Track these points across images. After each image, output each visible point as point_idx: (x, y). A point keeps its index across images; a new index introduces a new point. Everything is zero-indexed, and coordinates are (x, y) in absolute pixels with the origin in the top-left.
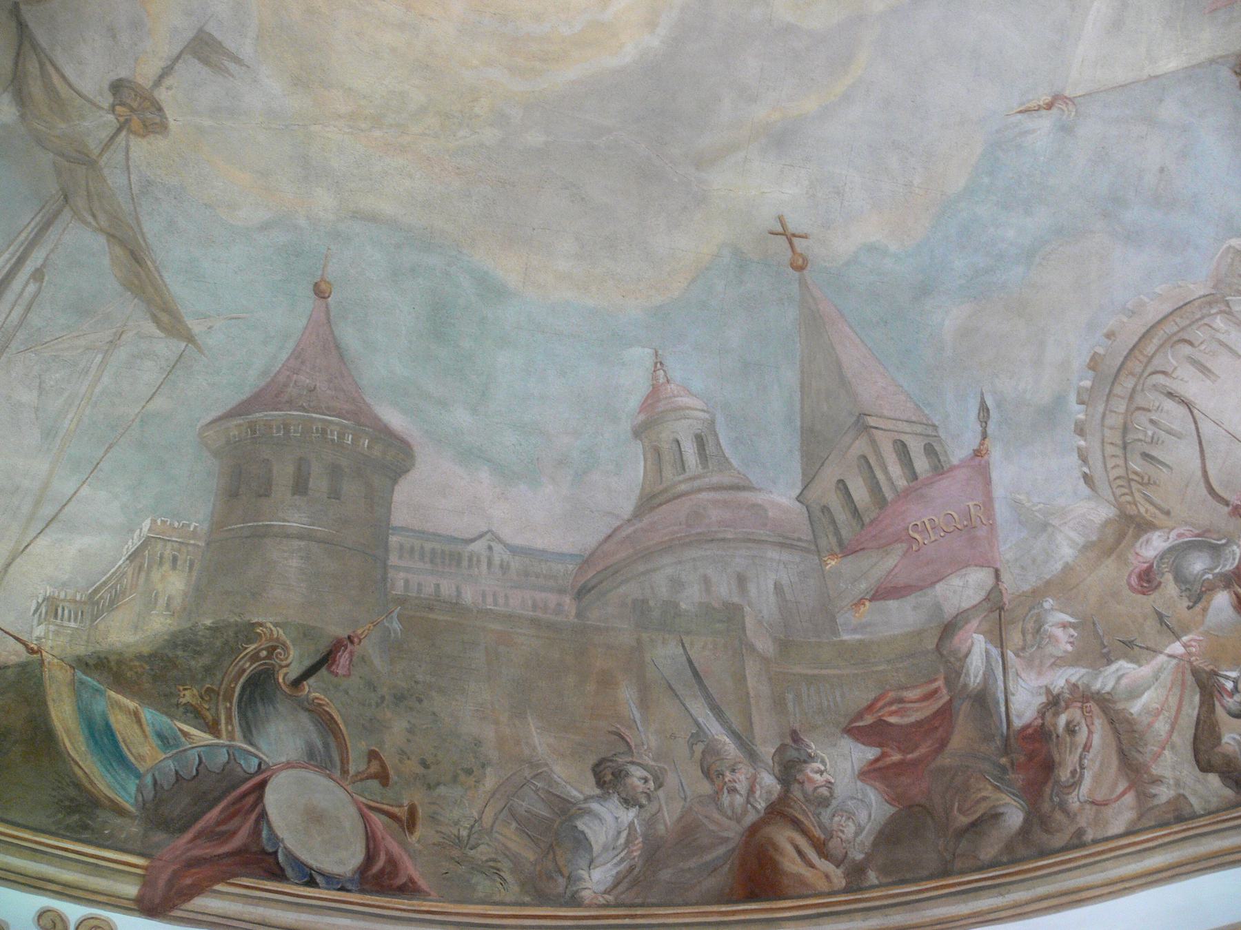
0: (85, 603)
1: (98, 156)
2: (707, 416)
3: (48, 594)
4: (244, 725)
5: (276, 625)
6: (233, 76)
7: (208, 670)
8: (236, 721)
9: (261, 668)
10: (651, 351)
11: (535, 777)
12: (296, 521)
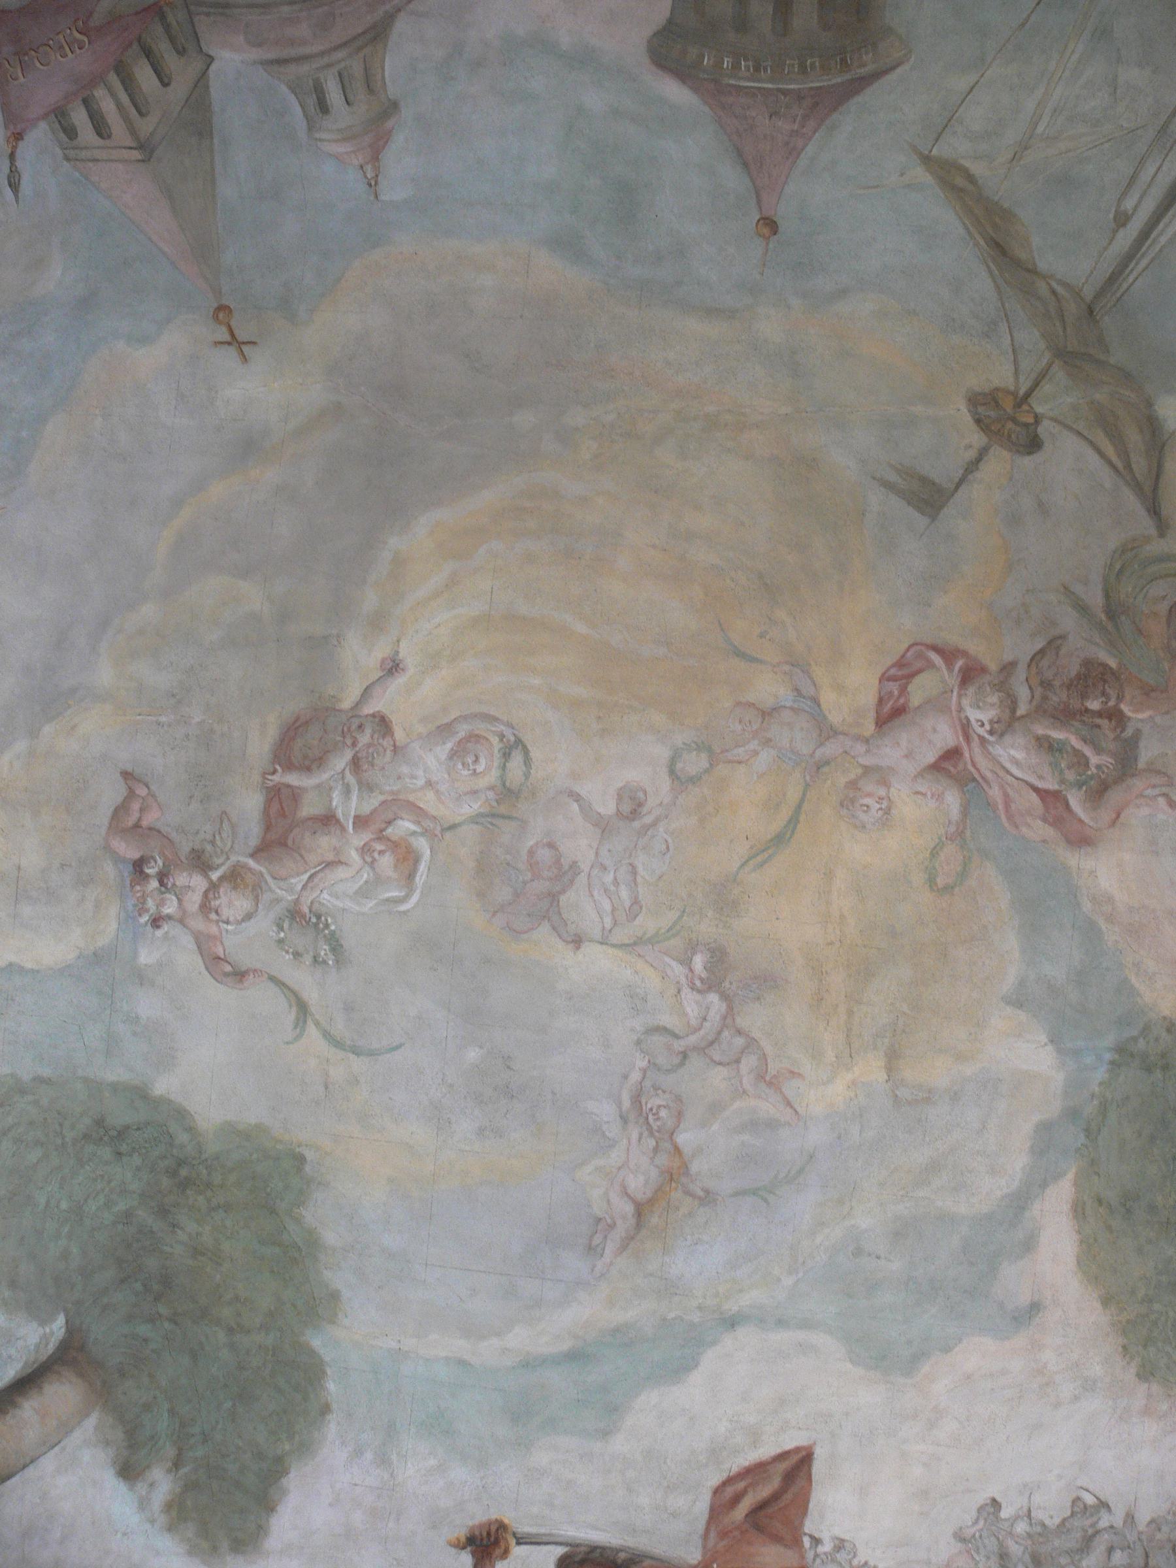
1: (1053, 363)
2: (317, 136)
10: (382, 197)
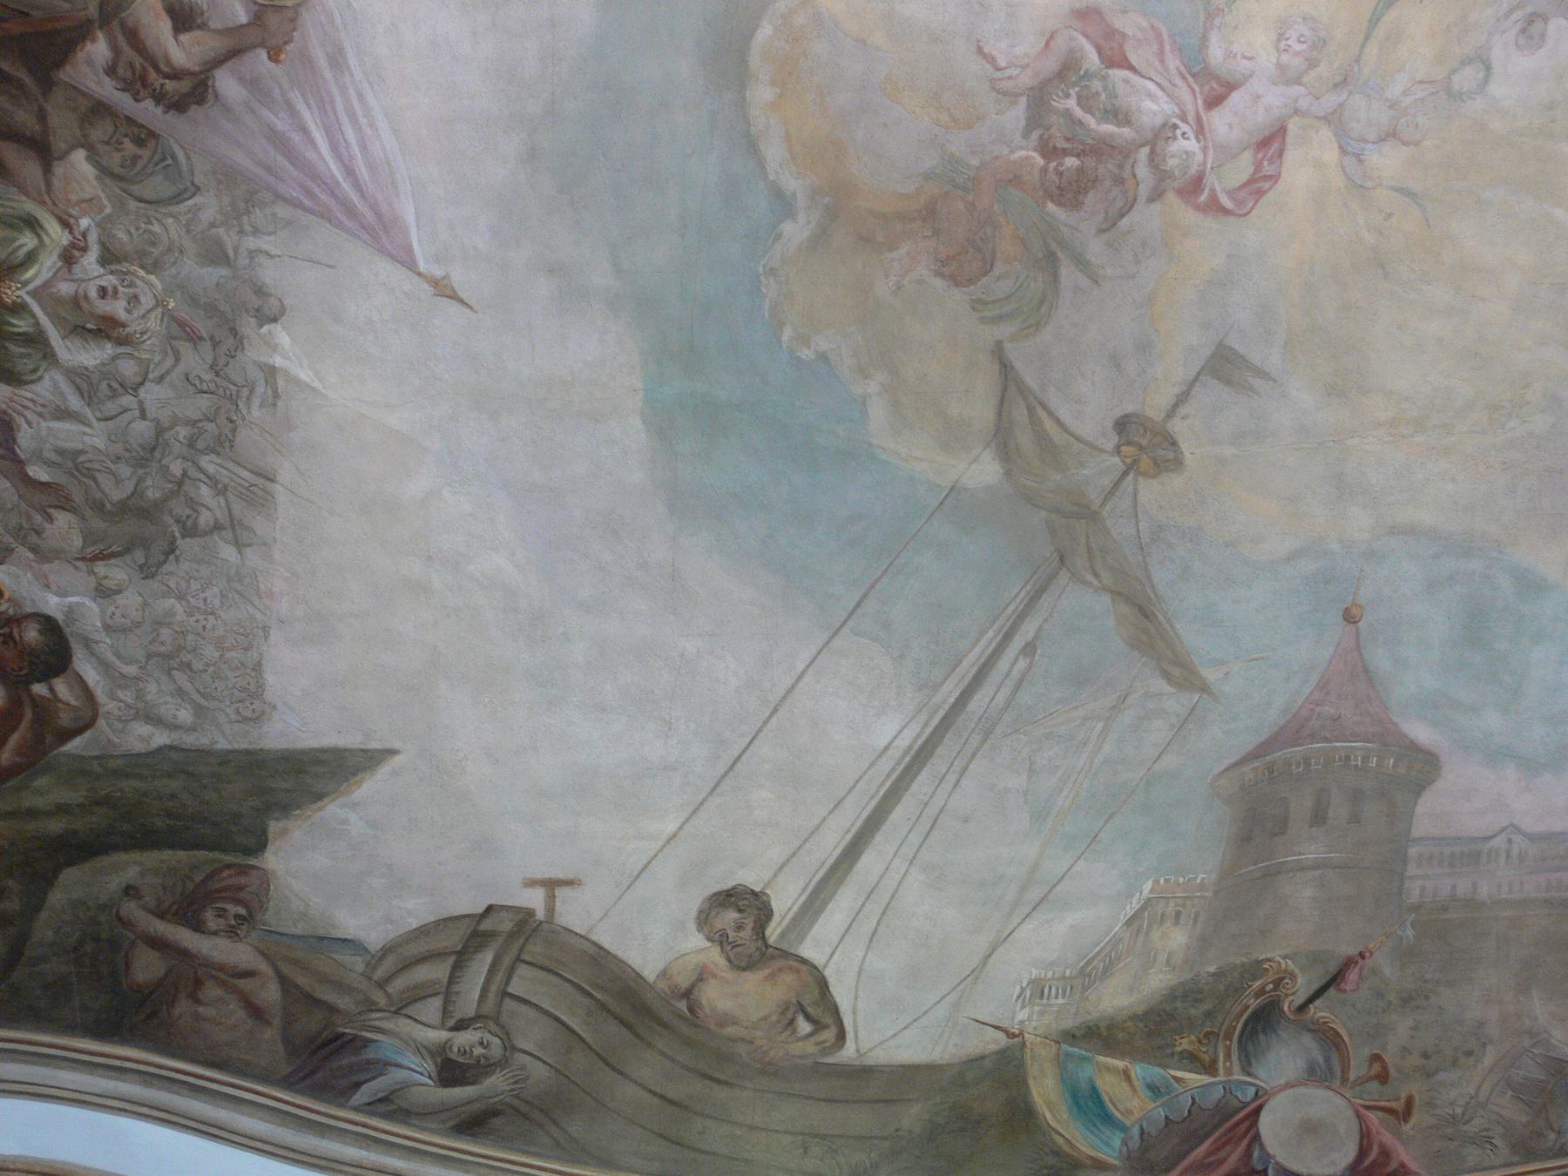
0: (1075, 978)
3: (1033, 977)
4: (1243, 1058)
5: (1285, 957)
6: (1257, 394)
7: (1209, 1015)
8: (1235, 1057)
9: (1267, 1000)
11: (1533, 1046)
12: (1312, 850)
